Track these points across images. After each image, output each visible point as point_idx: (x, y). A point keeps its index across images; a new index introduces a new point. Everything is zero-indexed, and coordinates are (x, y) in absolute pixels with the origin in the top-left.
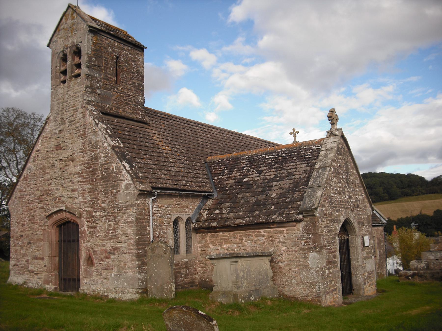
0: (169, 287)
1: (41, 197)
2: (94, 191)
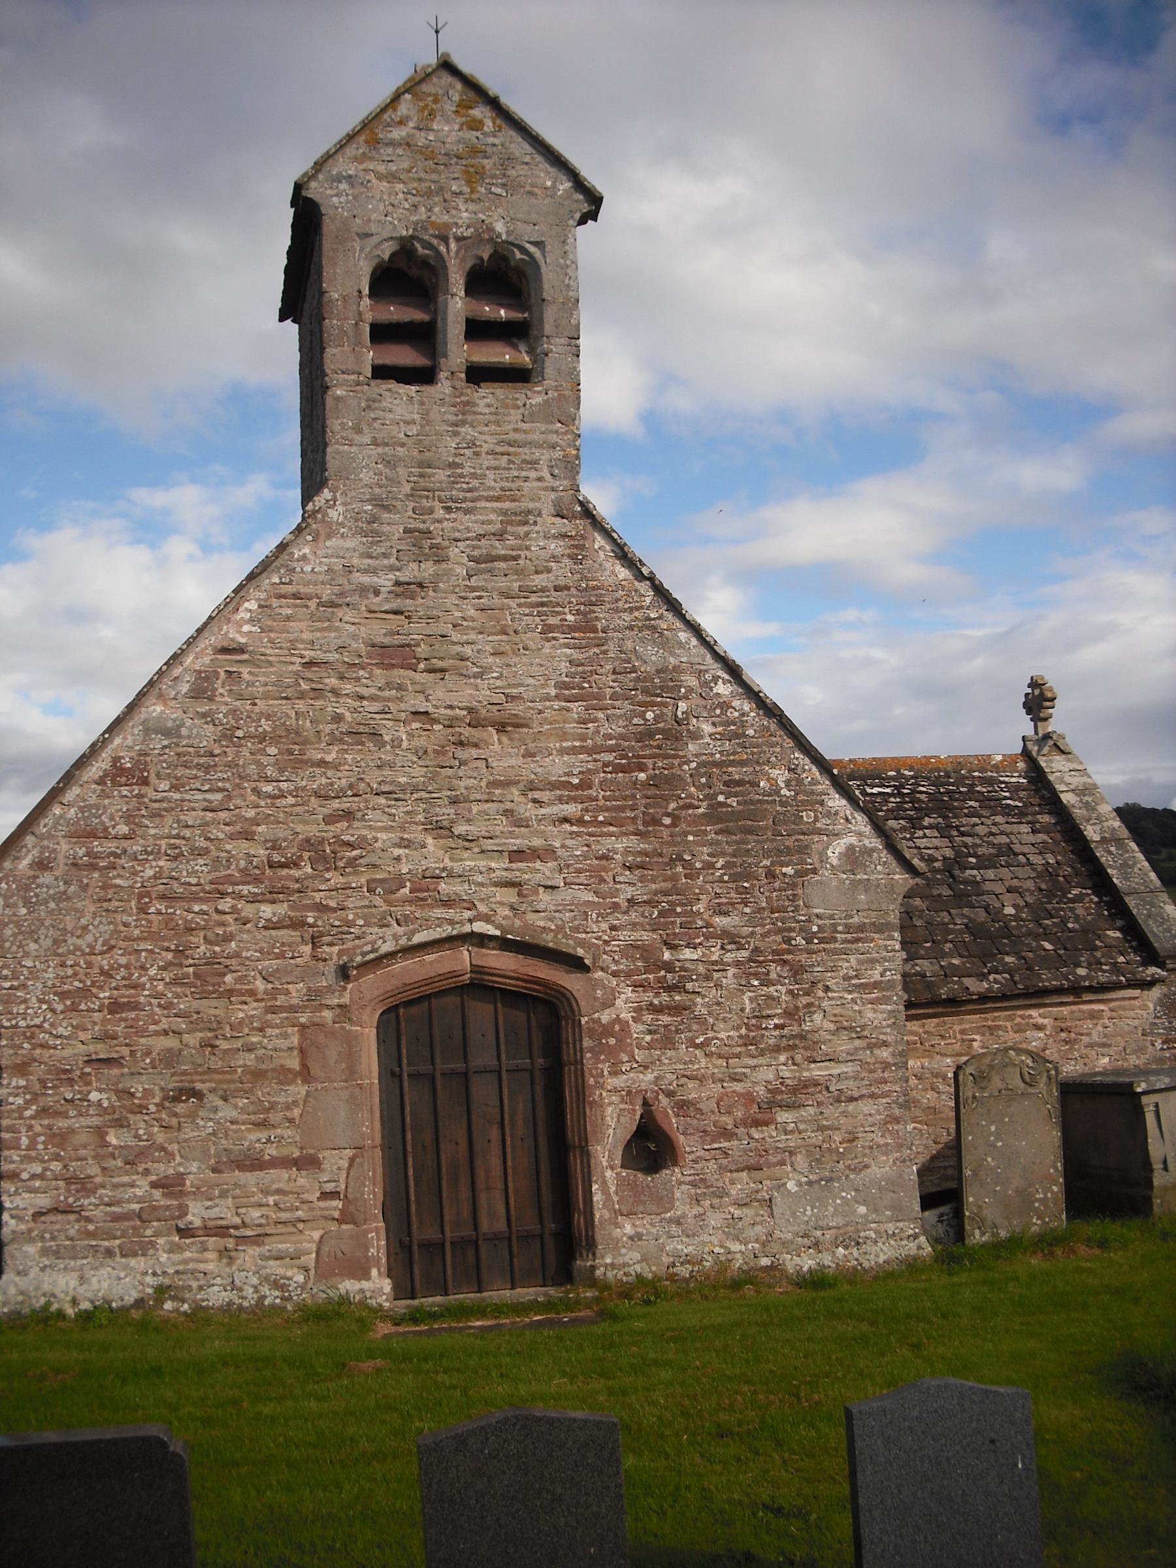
0: (1053, 1192)
1: (268, 871)
2: (667, 864)
